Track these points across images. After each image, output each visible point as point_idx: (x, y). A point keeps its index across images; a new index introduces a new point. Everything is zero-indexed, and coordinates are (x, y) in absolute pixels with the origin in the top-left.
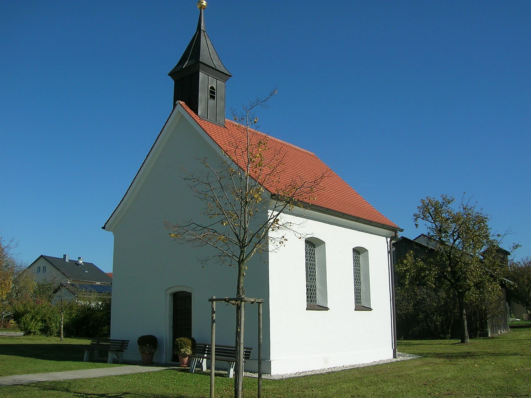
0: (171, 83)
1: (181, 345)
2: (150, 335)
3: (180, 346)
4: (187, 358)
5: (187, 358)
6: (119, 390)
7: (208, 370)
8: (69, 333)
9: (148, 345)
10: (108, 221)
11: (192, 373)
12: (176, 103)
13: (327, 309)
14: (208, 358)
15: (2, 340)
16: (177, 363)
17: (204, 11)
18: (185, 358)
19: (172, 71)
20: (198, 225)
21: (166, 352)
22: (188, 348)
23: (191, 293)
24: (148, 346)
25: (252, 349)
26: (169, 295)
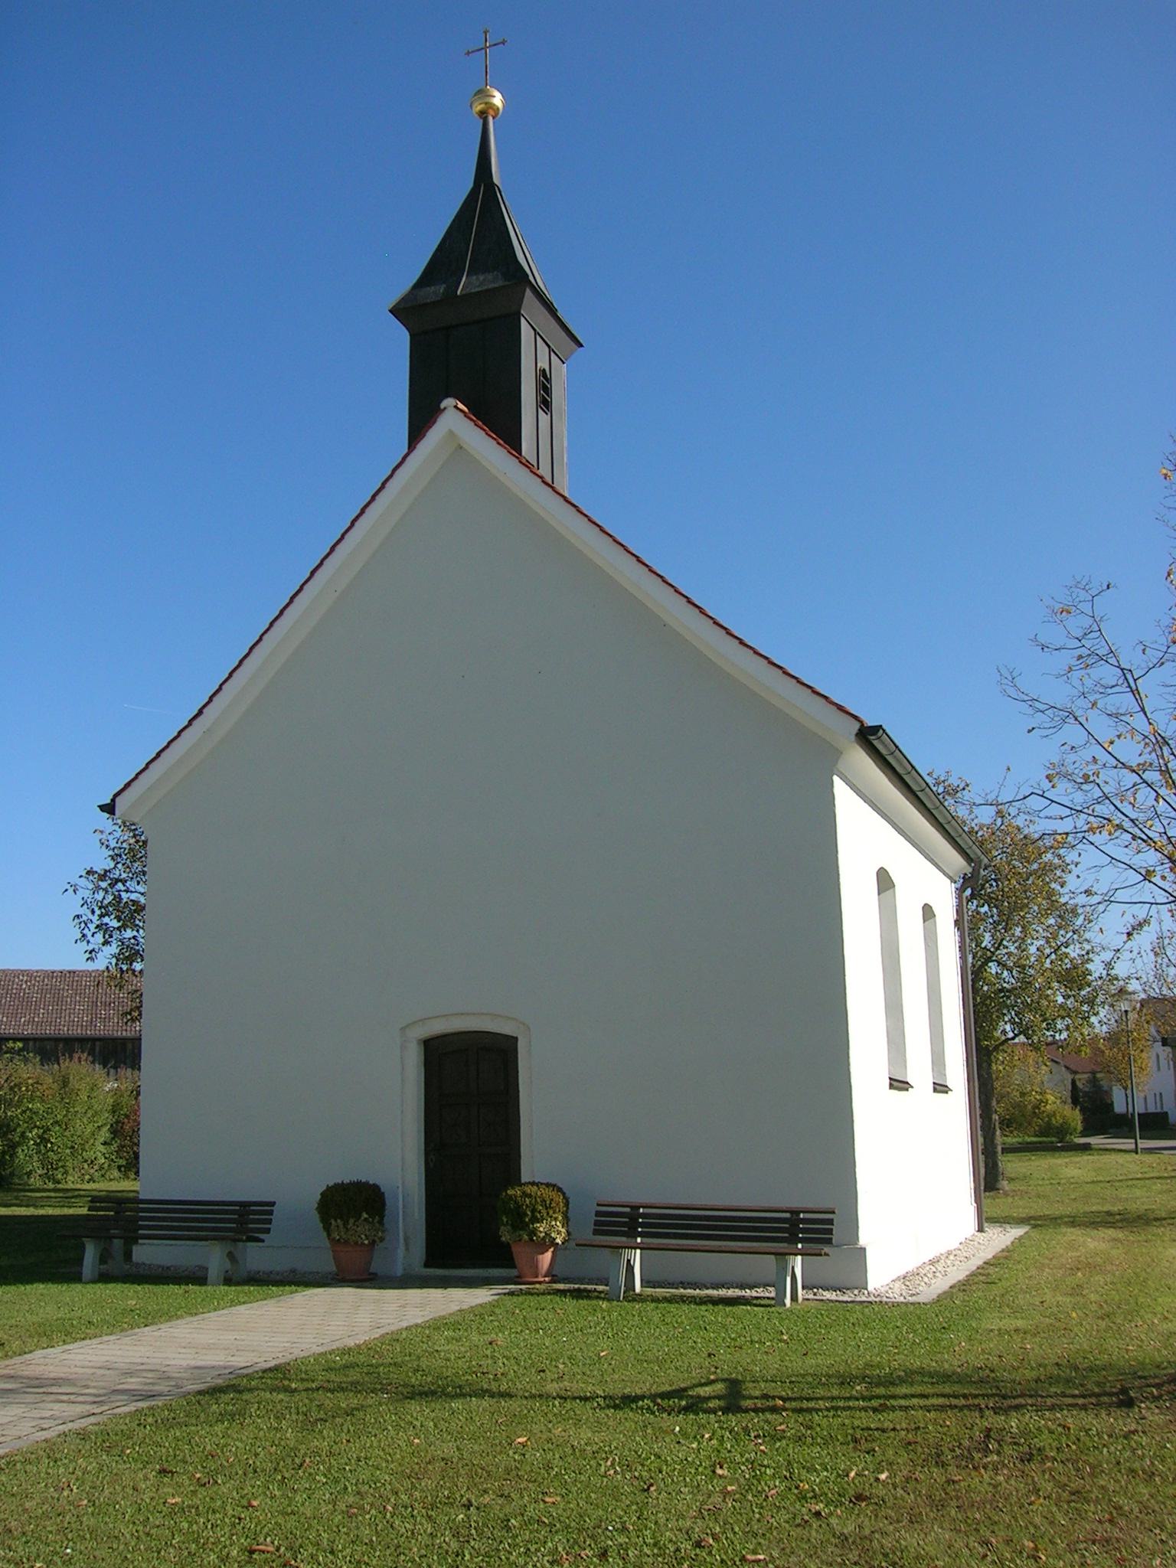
0: (399, 339)
1: (533, 1211)
2: (331, 1184)
3: (529, 1213)
4: (548, 1255)
5: (548, 1255)
6: (912, 1335)
7: (644, 1289)
8: (1037, 1136)
9: (365, 1215)
10: (128, 785)
11: (619, 1301)
12: (442, 406)
13: (906, 1086)
14: (645, 1246)
15: (4, 1209)
16: (514, 1272)
17: (494, 123)
18: (543, 1253)
19: (403, 300)
20: (1053, 801)
21: (406, 1239)
22: (556, 1219)
23: (516, 1039)
24: (366, 1219)
25: (834, 1213)
26: (415, 1042)
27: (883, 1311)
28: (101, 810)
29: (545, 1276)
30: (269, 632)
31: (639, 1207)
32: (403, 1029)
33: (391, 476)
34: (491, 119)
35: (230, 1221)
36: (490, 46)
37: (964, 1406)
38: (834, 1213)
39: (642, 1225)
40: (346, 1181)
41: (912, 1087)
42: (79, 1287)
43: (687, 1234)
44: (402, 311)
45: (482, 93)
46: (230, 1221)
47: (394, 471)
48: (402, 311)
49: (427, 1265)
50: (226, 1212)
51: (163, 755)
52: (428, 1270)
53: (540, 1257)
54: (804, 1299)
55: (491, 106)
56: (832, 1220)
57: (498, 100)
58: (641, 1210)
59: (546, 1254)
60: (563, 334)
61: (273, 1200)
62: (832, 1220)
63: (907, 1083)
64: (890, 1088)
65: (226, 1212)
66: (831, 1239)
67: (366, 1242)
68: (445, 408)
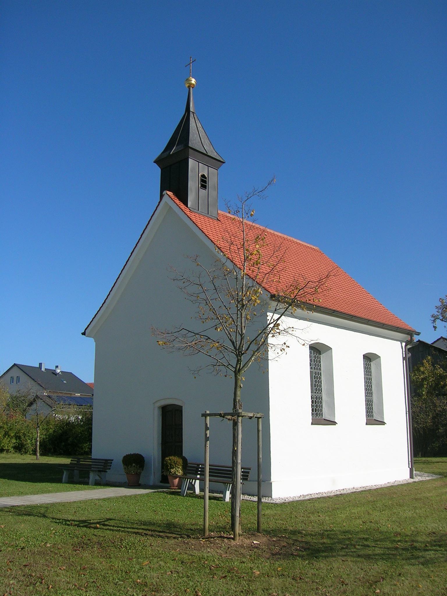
0: (157, 171)
1: (171, 465)
4: (177, 480)
9: (134, 465)
10: (88, 326)
13: (384, 423)
17: (193, 90)
20: (189, 331)
22: (179, 468)
23: (182, 407)
24: (134, 466)
27: (276, 505)
28: (82, 335)
29: (176, 487)
30: (121, 274)
31: (200, 465)
32: (154, 403)
33: (151, 219)
34: (191, 88)
35: (101, 465)
36: (192, 62)
37: (123, 531)
38: (250, 469)
39: (200, 471)
40: (132, 453)
41: (386, 424)
42: (61, 484)
43: (226, 476)
44: (158, 162)
45: (188, 80)
46: (101, 465)
47: (152, 217)
48: (158, 162)
49: (161, 482)
50: (100, 462)
51: (97, 316)
52: (161, 484)
53: (174, 480)
54: (242, 499)
55: (191, 84)
56: (249, 472)
57: (193, 81)
58: (200, 466)
59: (176, 479)
60: (214, 160)
61: (113, 459)
62: (249, 472)
63: (335, 422)
64: (311, 425)
65: (100, 462)
66: (247, 479)
67: (133, 473)
68: (162, 196)
